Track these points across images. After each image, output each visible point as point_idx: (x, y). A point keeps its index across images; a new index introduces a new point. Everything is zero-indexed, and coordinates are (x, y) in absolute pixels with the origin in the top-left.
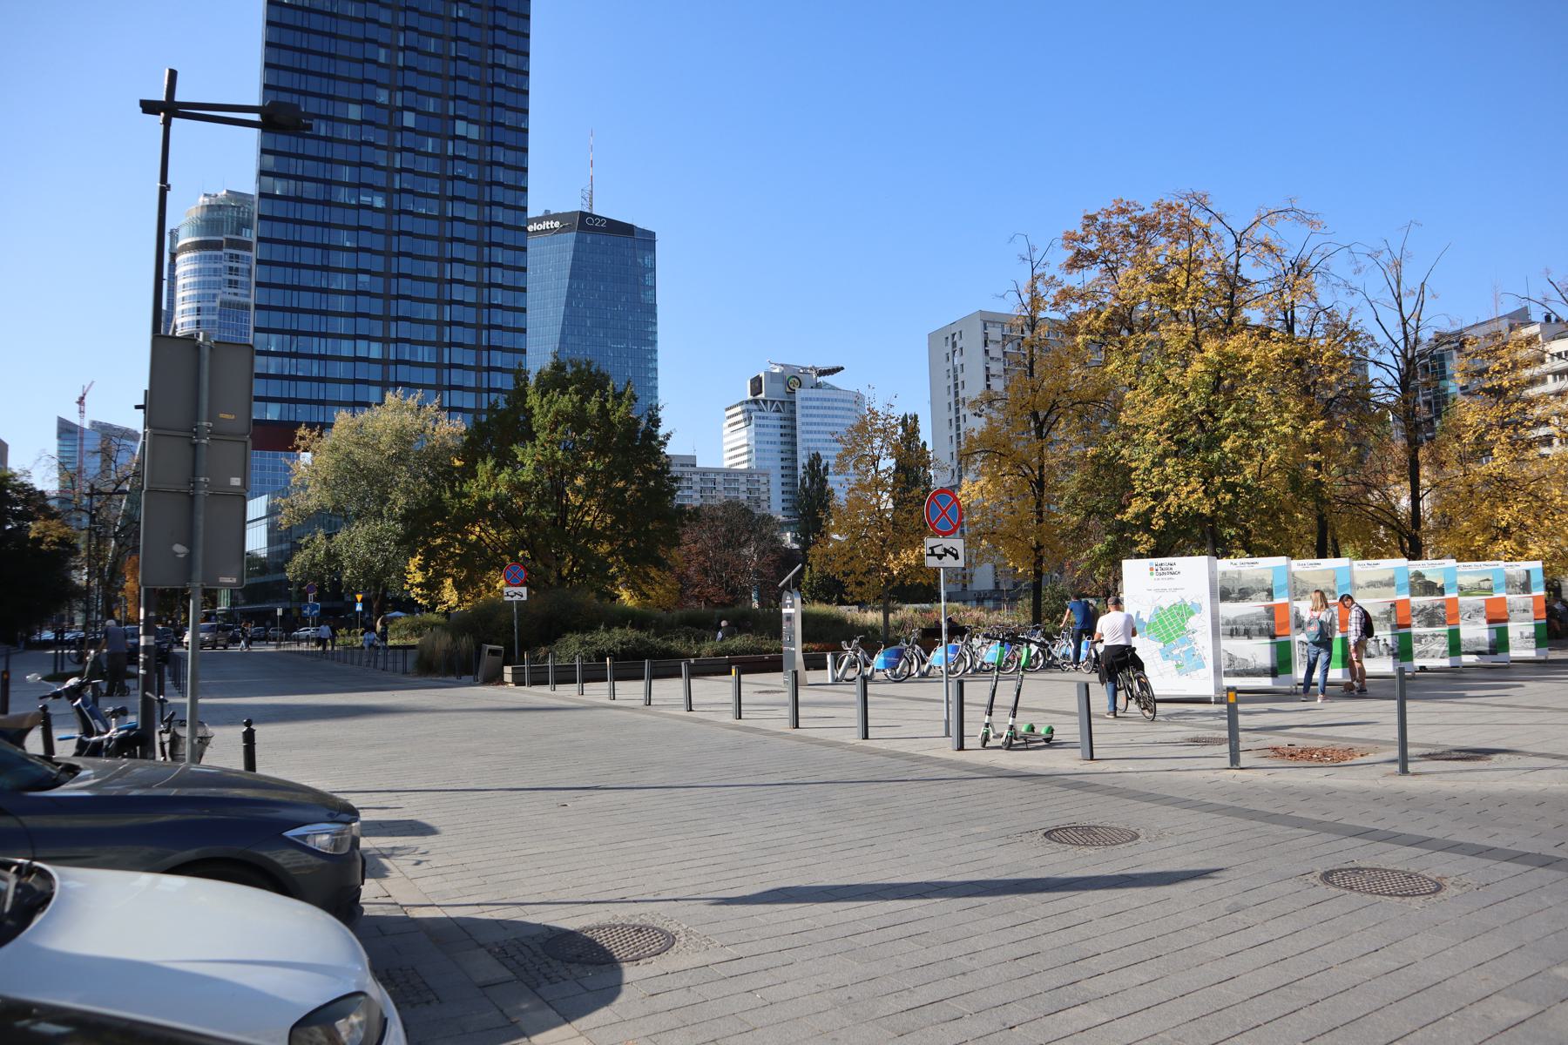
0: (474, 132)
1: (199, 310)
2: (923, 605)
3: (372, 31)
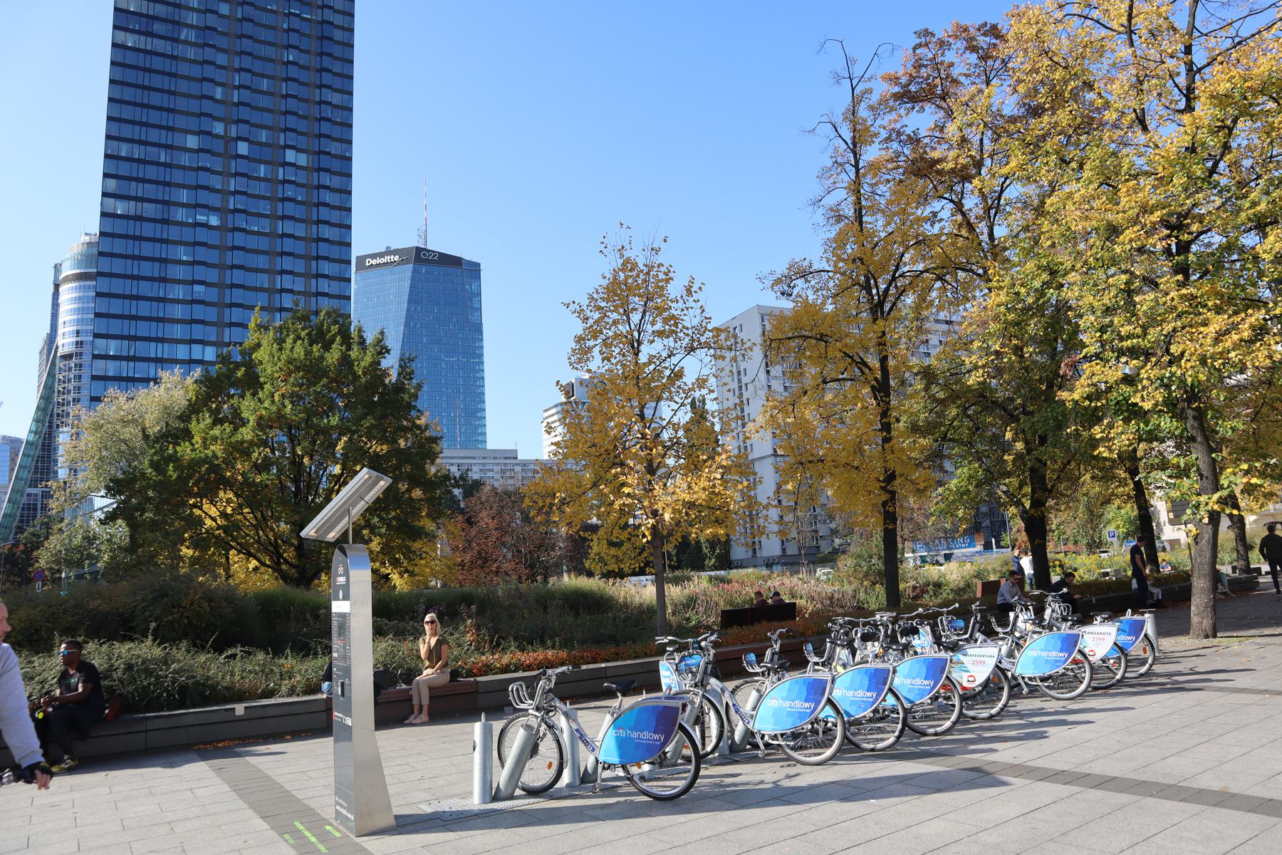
0: (302, 160)
1: (78, 332)
2: (718, 572)
3: (209, 71)
